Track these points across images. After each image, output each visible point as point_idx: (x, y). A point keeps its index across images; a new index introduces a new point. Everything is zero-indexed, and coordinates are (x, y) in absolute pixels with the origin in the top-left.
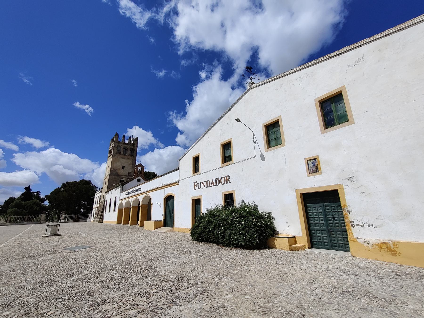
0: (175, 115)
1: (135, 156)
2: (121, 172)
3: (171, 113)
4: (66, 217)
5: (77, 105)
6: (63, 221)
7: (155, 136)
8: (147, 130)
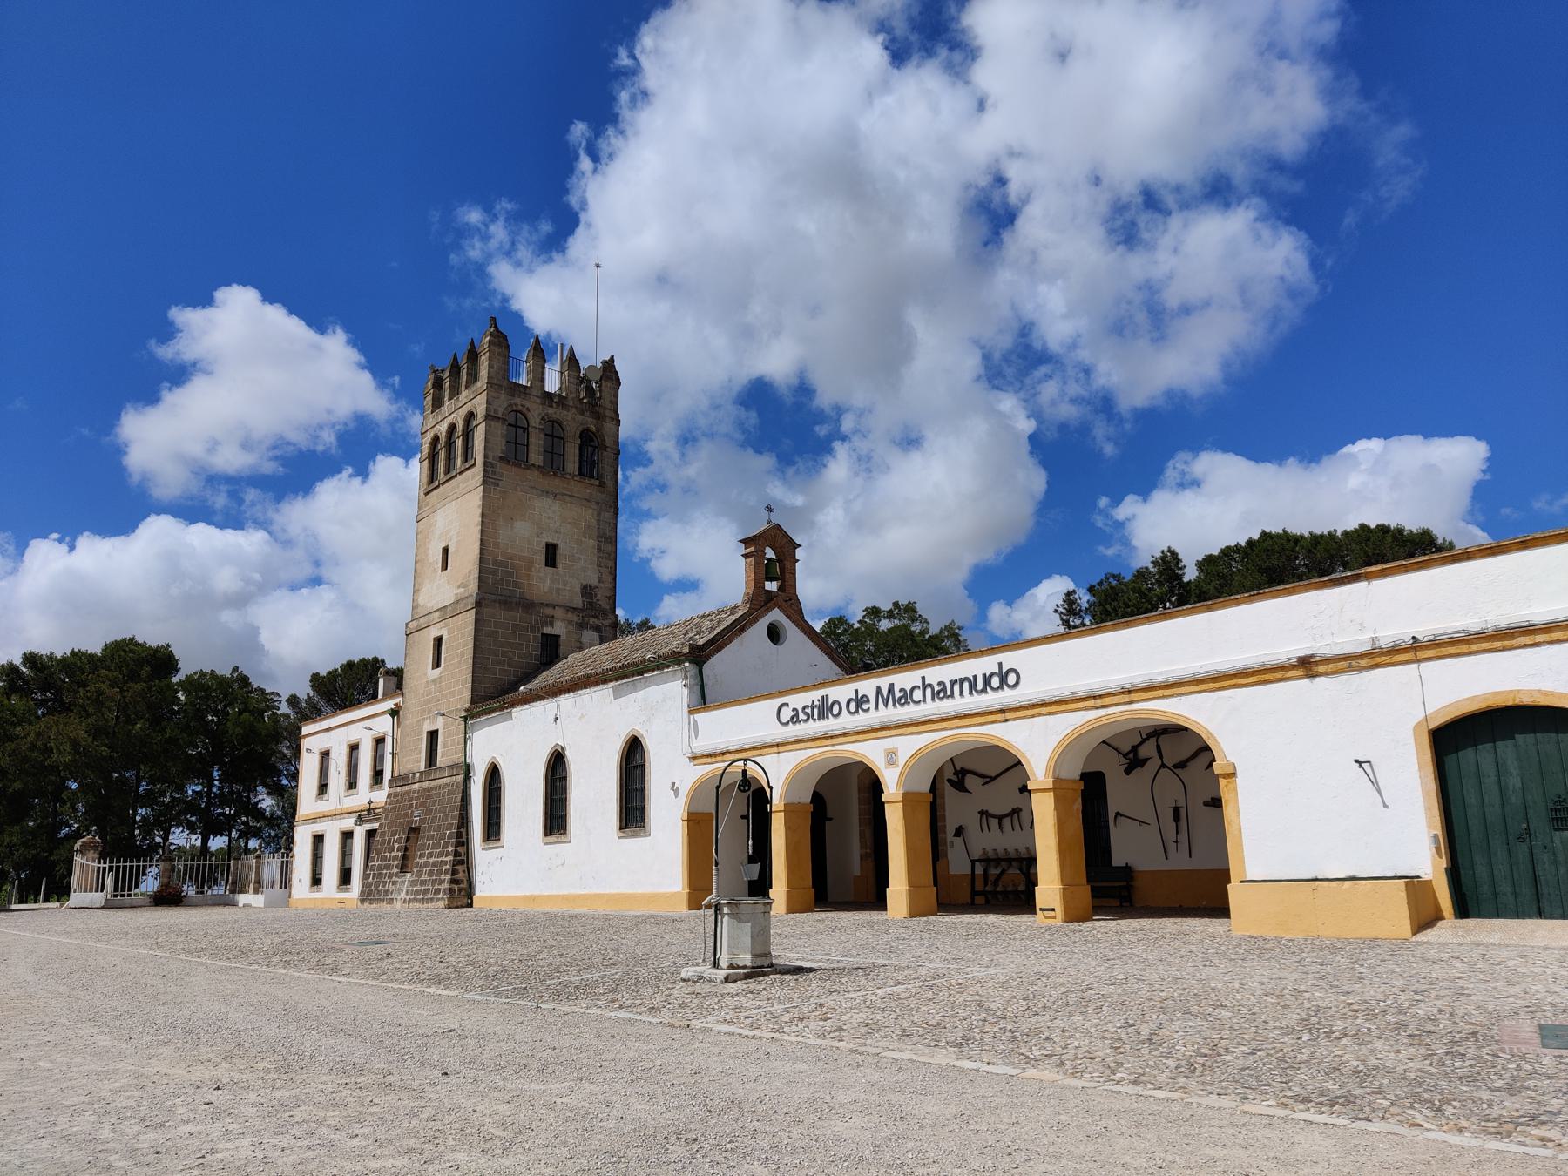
0: (499, 231)
1: (610, 484)
2: (542, 583)
3: (474, 216)
4: (101, 874)
6: (97, 898)
7: (377, 361)
8: (318, 324)
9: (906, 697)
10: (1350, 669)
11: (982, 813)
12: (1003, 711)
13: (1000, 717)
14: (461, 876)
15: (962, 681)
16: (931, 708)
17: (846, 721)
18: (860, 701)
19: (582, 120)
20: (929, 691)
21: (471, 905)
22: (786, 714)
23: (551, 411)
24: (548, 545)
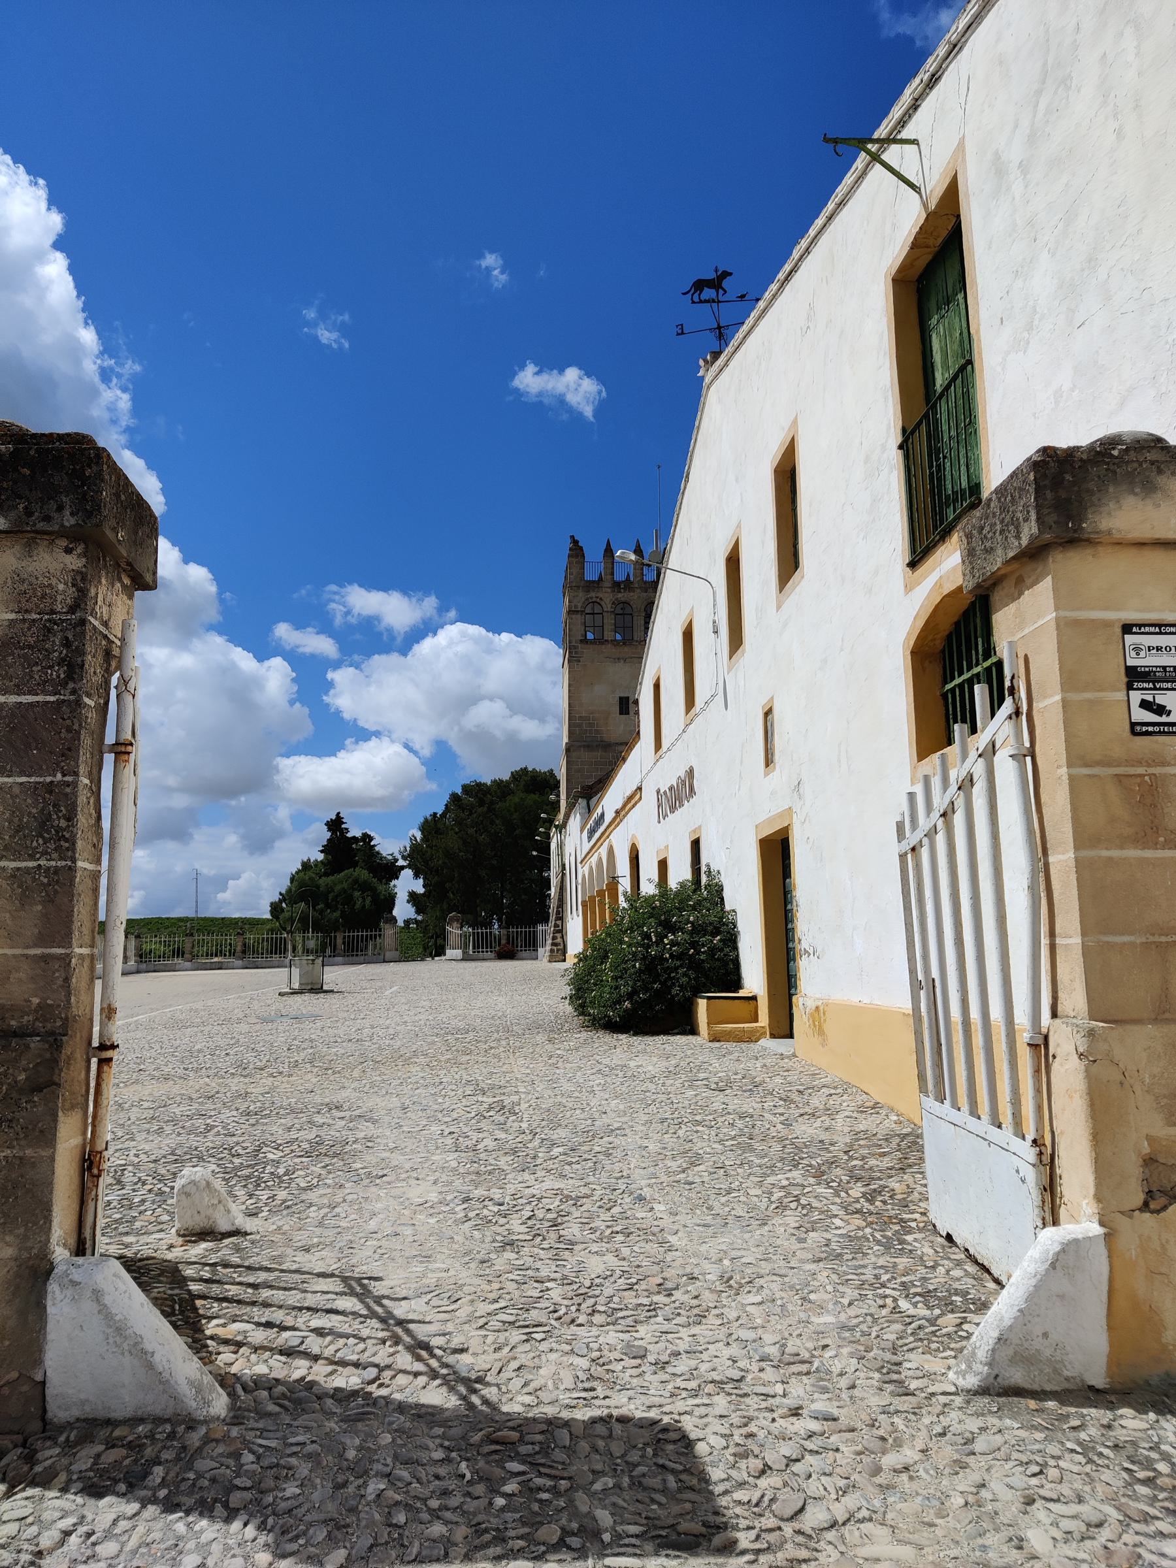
4: (464, 936)
5: (529, 380)
6: (458, 953)
14: (559, 940)
19: (492, 252)
21: (564, 960)
23: (620, 595)
24: (621, 698)
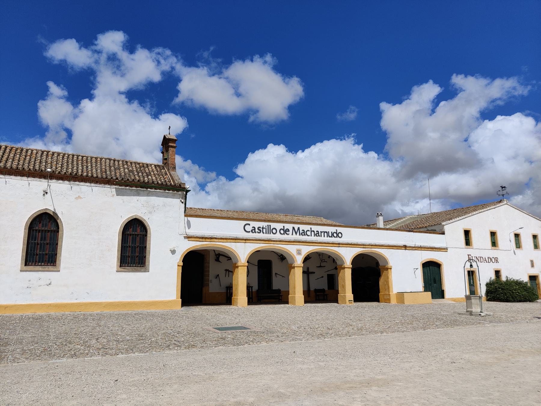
9: (304, 233)
10: (412, 250)
11: (226, 270)
12: (339, 244)
13: (338, 245)
15: (324, 232)
16: (313, 238)
17: (278, 236)
18: (286, 231)
20: (313, 233)
22: (248, 228)
